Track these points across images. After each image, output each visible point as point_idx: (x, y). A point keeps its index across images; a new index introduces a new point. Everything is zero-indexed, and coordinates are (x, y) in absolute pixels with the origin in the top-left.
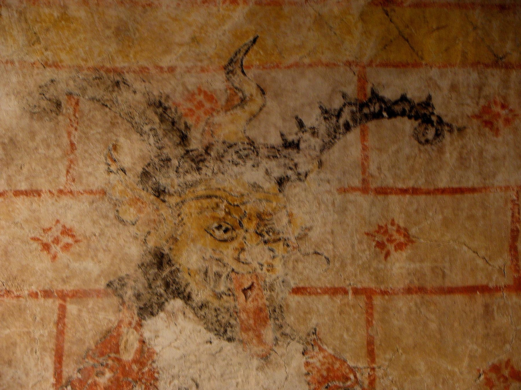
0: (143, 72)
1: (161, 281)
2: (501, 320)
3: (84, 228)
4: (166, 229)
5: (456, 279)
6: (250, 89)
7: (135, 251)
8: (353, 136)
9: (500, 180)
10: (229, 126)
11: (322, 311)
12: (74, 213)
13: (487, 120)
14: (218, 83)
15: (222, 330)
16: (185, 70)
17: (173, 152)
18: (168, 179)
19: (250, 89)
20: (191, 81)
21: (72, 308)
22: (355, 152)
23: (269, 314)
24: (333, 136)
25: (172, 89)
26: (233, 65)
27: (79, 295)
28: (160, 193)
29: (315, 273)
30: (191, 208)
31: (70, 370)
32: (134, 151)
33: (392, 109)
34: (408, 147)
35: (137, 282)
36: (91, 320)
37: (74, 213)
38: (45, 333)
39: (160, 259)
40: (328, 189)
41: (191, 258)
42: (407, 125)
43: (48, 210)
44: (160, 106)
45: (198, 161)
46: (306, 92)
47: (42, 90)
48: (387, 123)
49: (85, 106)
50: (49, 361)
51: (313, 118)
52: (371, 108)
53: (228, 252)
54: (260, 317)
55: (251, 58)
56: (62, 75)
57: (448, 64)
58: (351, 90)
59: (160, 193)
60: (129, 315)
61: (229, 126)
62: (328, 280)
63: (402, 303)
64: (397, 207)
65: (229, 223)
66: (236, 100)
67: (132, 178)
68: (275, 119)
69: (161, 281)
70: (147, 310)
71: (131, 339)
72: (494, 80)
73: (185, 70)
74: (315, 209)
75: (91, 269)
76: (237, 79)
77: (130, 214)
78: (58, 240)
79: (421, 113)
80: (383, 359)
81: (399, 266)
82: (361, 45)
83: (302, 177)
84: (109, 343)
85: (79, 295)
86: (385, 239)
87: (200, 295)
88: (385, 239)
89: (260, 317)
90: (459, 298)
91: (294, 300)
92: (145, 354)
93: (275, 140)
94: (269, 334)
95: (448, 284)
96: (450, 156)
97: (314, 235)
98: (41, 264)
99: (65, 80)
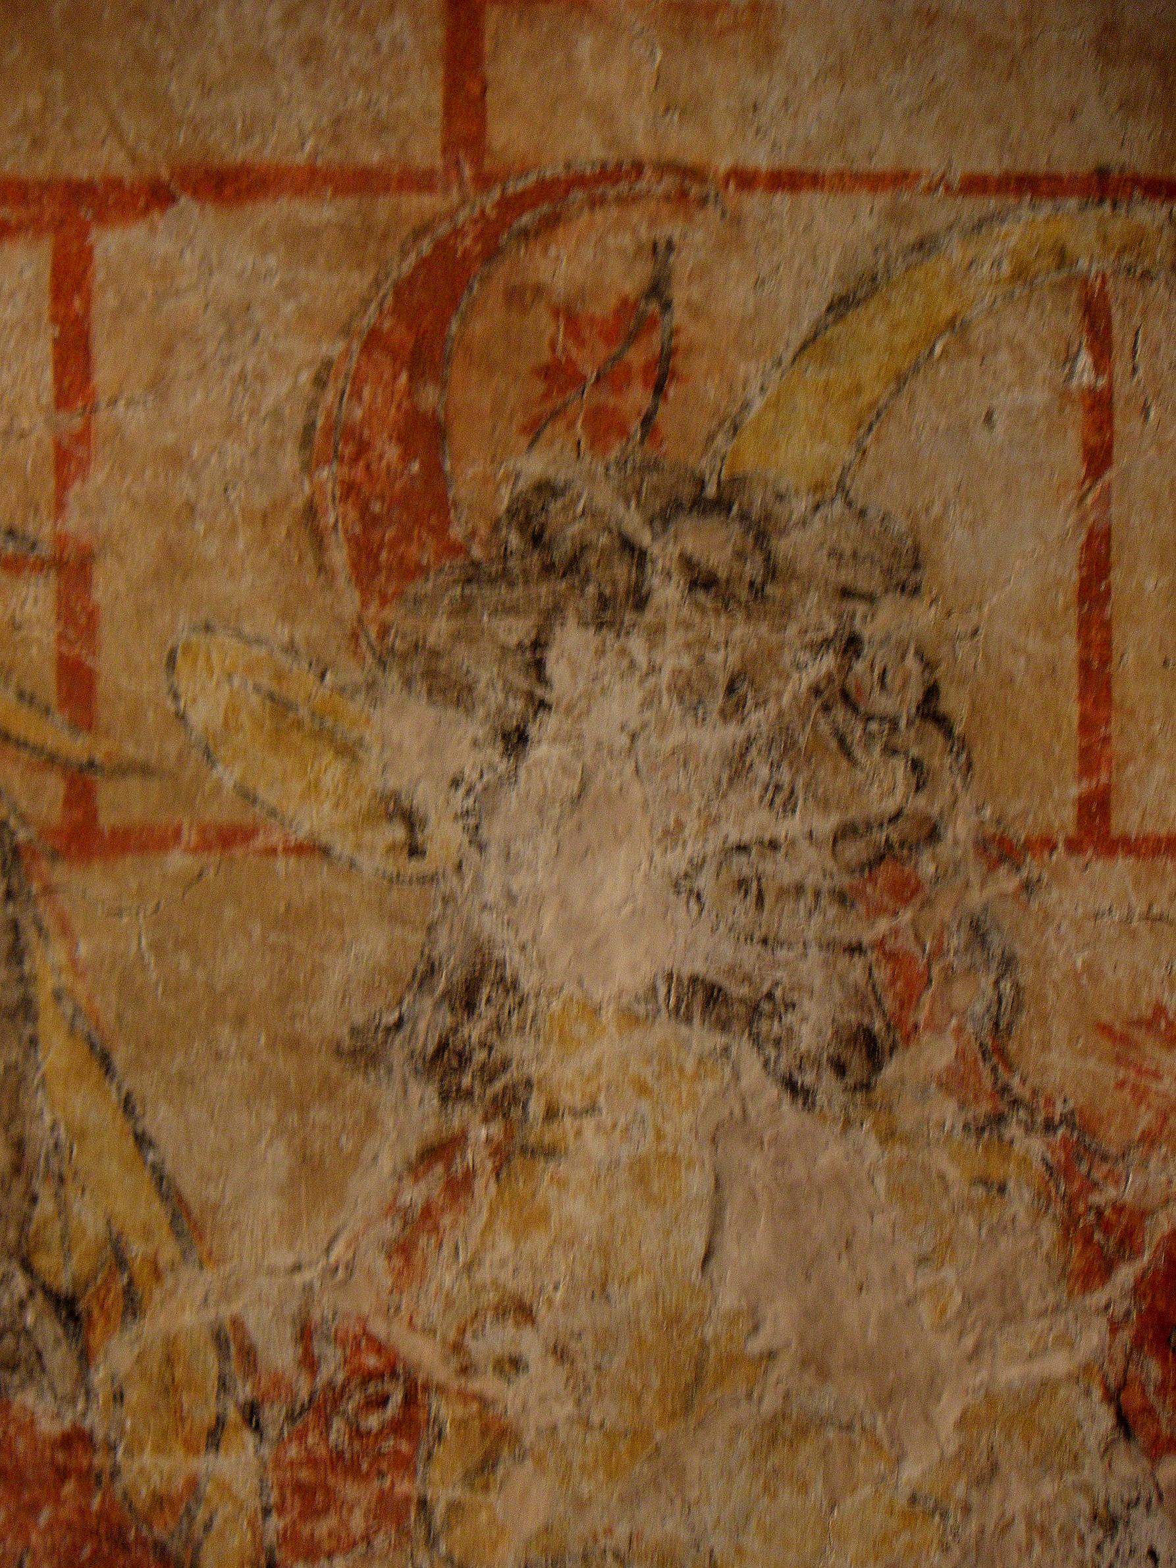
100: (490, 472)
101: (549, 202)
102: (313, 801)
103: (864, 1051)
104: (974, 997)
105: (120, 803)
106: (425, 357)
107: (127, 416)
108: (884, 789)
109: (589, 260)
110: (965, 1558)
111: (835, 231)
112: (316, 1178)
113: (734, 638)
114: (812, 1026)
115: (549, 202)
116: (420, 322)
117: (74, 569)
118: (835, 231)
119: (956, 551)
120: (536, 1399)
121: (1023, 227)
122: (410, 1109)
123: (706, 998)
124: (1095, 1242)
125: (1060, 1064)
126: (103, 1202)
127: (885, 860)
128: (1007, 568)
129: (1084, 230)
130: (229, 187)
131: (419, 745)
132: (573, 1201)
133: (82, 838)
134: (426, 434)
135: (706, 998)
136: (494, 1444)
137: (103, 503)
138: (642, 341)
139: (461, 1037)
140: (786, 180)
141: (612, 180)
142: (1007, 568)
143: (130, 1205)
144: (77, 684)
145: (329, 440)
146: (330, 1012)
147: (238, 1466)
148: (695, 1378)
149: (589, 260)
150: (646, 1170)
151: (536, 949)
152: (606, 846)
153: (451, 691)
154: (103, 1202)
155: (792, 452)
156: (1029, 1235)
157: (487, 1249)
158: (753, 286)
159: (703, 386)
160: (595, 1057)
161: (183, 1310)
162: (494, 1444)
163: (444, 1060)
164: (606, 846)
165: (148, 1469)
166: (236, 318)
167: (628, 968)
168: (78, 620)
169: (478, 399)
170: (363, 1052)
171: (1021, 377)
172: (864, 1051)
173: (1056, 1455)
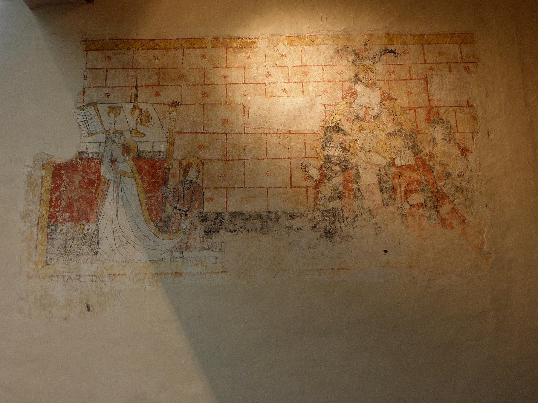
0: (351, 46)
1: (357, 79)
2: (409, 85)
3: (344, 71)
4: (357, 71)
5: (401, 78)
6: (368, 48)
7: (352, 74)
8: (384, 56)
9: (407, 63)
10: (365, 54)
11: (382, 83)
12: (342, 68)
13: (405, 53)
14: (363, 47)
15: (367, 86)
16: (358, 45)
17: (357, 58)
18: (357, 63)
19: (368, 48)
20: (359, 47)
21: (344, 83)
22: (385, 58)
23: (374, 84)
24: (381, 55)
25: (356, 49)
26: (365, 44)
27: (345, 81)
28: (355, 65)
29: (380, 77)
30: (360, 67)
31: (344, 93)
32: (351, 58)
33: (390, 52)
34: (393, 57)
35: (353, 79)
36: (347, 85)
37: (342, 68)
38: (340, 87)
39: (356, 76)
40: (368, 214)
41: (361, 75)
42: (392, 54)
43: (338, 68)
44: (354, 51)
45: (361, 60)
46: (377, 49)
47: (336, 49)
48: (389, 54)
49: (343, 51)
50: (341, 91)
51: (378, 53)
52: (387, 51)
53: (367, 74)
54: (372, 84)
55: (368, 43)
56: (339, 46)
57: (398, 44)
58: (384, 48)
59: (355, 65)
60: (353, 84)
61: (365, 54)
62: (382, 79)
63: (394, 82)
64: (392, 67)
65: (367, 69)
66: (366, 50)
67: (351, 63)
68: (372, 53)
69: (357, 79)
70: (355, 84)
71: (353, 88)
72: (405, 47)
73: (358, 45)
74: (379, 67)
75: (346, 77)
76: (366, 47)
77: (351, 69)
78: (340, 73)
79: (394, 52)
80: (391, 91)
81: (393, 76)
82: (385, 41)
83: (377, 62)
84: (350, 89)
85: (345, 81)
86: (390, 72)
87: (363, 81)
88: (390, 72)
89: (372, 84)
90: (402, 81)
91: (377, 82)
92: (355, 90)
93: (372, 57)
94: (374, 87)
95: (203, 49)
96: (399, 59)
97: (379, 71)
98: (338, 76)
99: (339, 47)
100: (432, 118)
101: (433, 108)
102: (427, 132)
103: (450, 141)
104: (454, 138)
105: (420, 132)
106: (429, 114)
107: (418, 117)
108: (449, 130)
109: (435, 110)
110: (427, 82)
111: (445, 108)
112: (429, 146)
113: (443, 125)
114: (448, 140)
115: (433, 108)
116: (429, 112)
117: (417, 123)
118: (445, 108)
119: (451, 121)
120: (439, 155)
121: (452, 108)
122: (432, 144)
123: (443, 139)
124: (460, 148)
125: (457, 141)
126: (421, 148)
127: (450, 133)
128: (453, 122)
129: (454, 108)
130: (421, 107)
131: (431, 129)
132: (439, 147)
133: (418, 133)
134: (429, 117)
135: (443, 139)
136: (437, 157)
137: (417, 120)
138: (437, 113)
139: (434, 140)
140: (179, 133)
141: (436, 107)
142: (453, 122)
143: (422, 148)
144: (417, 127)
145: (426, 117)
146: (429, 140)
147: (427, 158)
148: (445, 154)
149: (435, 110)
150: (442, 146)
151: (436, 137)
152: (439, 133)
153: (432, 127)
154: (421, 148)
155: (444, 117)
156: (457, 148)
157: (436, 149)
158: (441, 111)
159: (440, 115)
160: (439, 141)
161: (424, 152)
162: (437, 157)
163: (433, 142)
164: (439, 133)
165: (424, 158)
166: (422, 113)
167: (440, 138)
168: (417, 125)
169: (431, 115)
170: (430, 141)
171: (452, 114)
172: (450, 141)
173: (459, 156)
